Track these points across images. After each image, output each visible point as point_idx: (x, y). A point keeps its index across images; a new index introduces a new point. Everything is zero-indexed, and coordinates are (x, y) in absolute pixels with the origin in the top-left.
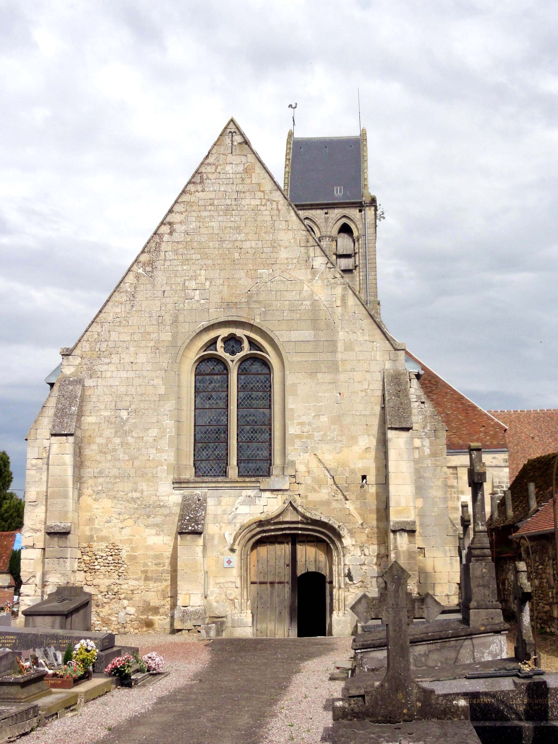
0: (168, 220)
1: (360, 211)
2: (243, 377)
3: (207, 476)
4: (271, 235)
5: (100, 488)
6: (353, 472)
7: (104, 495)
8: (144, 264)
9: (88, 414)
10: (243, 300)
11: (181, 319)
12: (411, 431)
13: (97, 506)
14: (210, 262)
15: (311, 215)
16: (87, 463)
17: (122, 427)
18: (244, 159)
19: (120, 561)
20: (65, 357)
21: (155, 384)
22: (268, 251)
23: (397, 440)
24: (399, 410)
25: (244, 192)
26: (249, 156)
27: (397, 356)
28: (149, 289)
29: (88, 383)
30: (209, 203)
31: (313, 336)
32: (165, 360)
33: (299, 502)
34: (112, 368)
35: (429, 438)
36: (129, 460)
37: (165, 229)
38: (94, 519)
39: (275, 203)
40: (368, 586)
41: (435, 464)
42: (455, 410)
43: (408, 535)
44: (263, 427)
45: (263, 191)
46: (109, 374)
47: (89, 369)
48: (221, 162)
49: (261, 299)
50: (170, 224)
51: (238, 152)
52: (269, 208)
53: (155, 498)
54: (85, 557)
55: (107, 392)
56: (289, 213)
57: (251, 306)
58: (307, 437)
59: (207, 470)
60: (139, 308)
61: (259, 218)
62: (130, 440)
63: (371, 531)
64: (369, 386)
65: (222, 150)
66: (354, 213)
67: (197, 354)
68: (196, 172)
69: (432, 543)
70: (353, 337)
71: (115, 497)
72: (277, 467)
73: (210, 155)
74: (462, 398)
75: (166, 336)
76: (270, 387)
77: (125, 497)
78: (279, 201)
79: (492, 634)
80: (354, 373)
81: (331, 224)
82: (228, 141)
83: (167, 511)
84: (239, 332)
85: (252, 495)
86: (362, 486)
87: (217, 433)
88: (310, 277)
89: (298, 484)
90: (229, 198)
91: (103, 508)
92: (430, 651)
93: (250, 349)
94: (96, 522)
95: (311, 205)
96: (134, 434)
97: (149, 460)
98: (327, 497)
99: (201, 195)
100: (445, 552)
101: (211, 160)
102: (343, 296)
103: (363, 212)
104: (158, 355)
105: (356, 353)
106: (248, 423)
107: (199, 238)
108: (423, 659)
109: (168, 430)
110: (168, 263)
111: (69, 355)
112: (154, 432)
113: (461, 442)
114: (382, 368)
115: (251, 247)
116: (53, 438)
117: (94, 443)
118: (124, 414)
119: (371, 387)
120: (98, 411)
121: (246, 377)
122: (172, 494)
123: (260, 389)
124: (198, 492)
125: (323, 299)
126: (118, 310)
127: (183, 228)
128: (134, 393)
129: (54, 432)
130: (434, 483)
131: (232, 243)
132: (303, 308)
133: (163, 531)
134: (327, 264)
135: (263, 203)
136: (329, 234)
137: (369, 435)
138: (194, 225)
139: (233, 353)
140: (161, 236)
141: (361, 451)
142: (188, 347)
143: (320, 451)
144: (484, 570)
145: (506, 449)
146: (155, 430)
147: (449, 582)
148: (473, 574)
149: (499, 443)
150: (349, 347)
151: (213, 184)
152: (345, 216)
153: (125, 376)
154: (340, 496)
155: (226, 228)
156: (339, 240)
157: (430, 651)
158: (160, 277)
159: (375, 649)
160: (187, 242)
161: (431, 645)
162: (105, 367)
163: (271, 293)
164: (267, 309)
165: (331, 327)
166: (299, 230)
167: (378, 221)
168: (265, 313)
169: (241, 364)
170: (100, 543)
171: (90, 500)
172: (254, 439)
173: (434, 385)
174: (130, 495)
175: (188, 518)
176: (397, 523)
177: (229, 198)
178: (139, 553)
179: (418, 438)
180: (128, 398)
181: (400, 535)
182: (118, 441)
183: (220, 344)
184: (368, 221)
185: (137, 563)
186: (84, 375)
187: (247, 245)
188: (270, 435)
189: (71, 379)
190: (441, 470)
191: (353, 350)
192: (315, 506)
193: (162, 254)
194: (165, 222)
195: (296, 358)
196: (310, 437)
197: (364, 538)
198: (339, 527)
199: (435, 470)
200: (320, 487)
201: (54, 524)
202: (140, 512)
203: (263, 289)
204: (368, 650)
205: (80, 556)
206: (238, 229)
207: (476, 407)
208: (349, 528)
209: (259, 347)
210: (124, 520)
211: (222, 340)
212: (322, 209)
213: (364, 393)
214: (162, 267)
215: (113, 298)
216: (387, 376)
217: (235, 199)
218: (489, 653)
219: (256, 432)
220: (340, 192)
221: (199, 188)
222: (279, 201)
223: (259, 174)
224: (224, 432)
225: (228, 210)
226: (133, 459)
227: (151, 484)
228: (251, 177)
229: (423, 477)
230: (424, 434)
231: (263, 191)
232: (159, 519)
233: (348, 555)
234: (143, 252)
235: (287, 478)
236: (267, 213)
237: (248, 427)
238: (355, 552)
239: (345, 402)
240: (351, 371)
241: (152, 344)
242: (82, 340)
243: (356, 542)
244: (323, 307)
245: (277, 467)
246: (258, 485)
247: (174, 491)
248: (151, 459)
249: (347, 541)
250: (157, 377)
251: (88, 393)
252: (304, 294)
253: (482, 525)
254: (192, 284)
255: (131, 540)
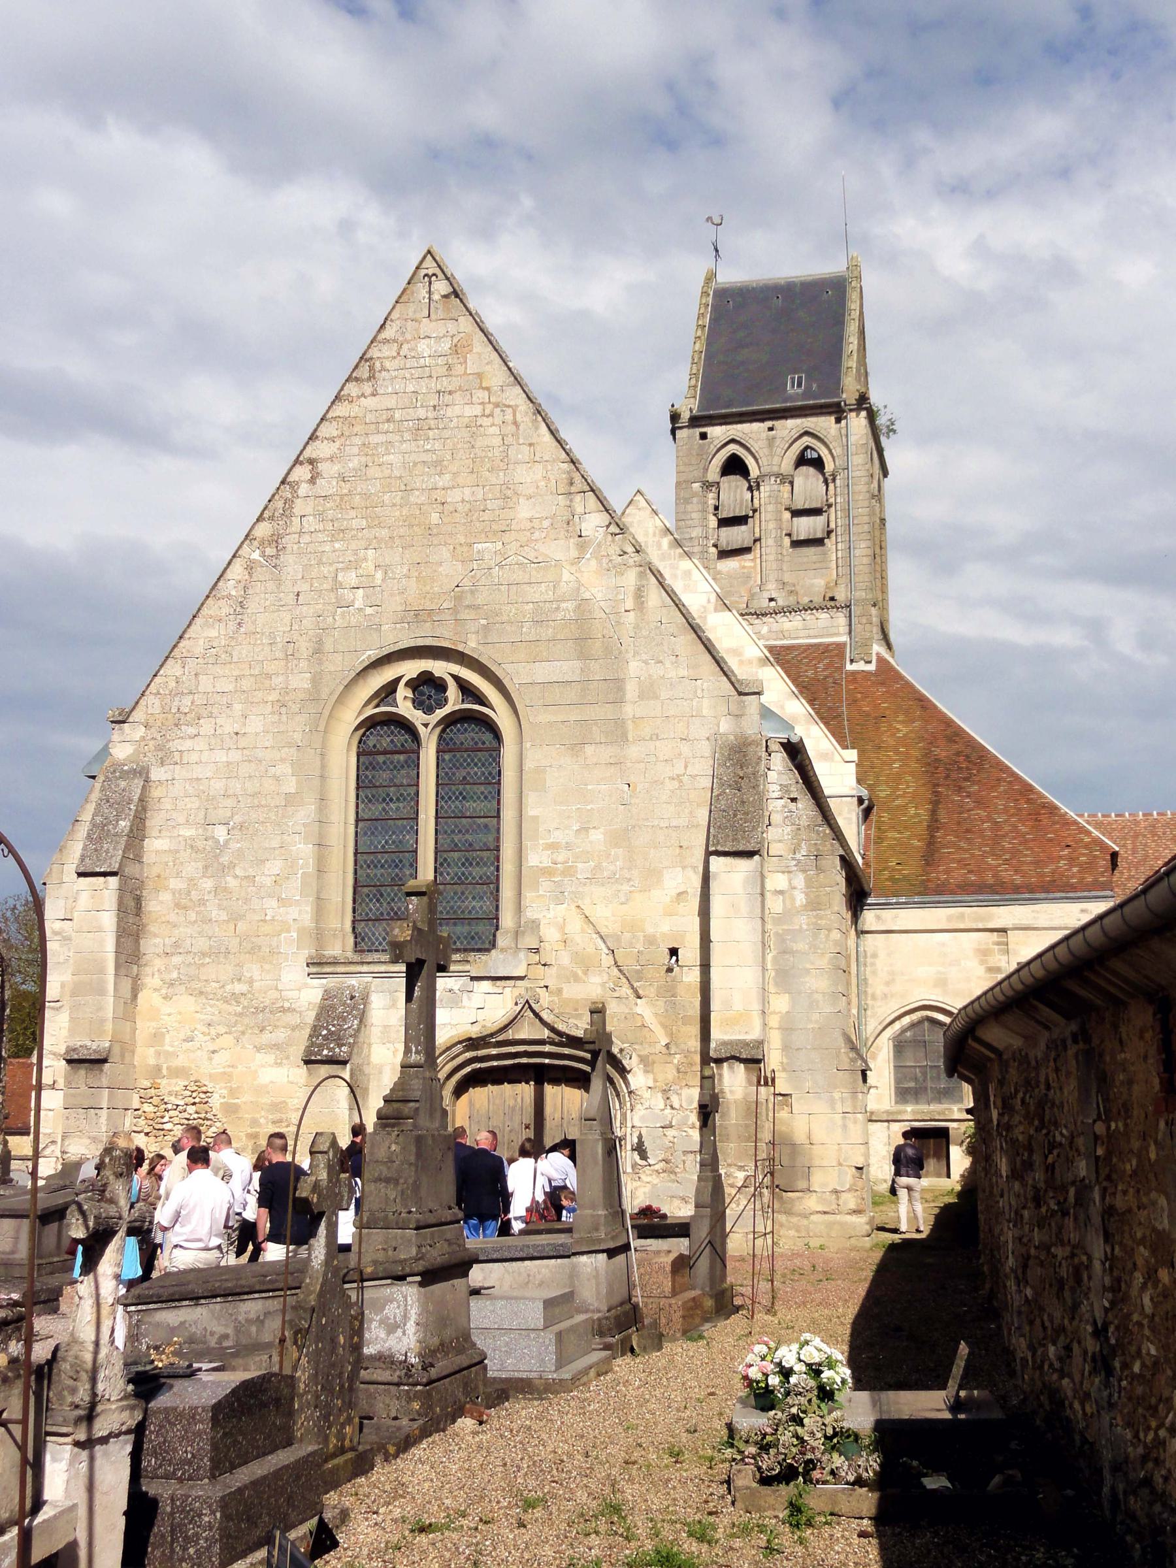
0: (307, 453)
1: (838, 421)
2: (447, 757)
3: (377, 951)
4: (501, 474)
5: (175, 975)
6: (651, 941)
7: (183, 988)
8: (262, 543)
9: (155, 833)
10: (445, 605)
11: (328, 646)
12: (757, 857)
13: (169, 1010)
14: (384, 533)
15: (740, 435)
16: (152, 928)
17: (216, 857)
18: (451, 327)
19: (209, 1116)
20: (117, 726)
21: (278, 774)
22: (495, 507)
23: (731, 875)
24: (735, 815)
25: (450, 393)
26: (461, 319)
27: (744, 707)
28: (269, 590)
29: (156, 774)
30: (384, 417)
31: (578, 672)
32: (297, 729)
33: (545, 1001)
34: (200, 744)
35: (804, 871)
36: (228, 921)
37: (302, 473)
38: (163, 1035)
39: (510, 411)
40: (677, 1170)
41: (816, 924)
42: (1012, 815)
43: (746, 1068)
44: (486, 854)
45: (488, 389)
46: (194, 757)
47: (159, 748)
48: (408, 336)
49: (479, 601)
50: (311, 462)
51: (441, 314)
52: (498, 421)
53: (276, 994)
54: (147, 1108)
55: (191, 791)
56: (537, 428)
57: (461, 616)
58: (564, 873)
59: (377, 939)
60: (252, 629)
61: (479, 443)
62: (231, 882)
63: (684, 1060)
64: (686, 767)
65: (410, 310)
66: (825, 424)
67: (360, 713)
68: (361, 358)
69: (808, 1085)
70: (656, 671)
71: (201, 993)
72: (507, 932)
73: (388, 322)
74: (1029, 789)
75: (301, 681)
76: (500, 775)
77: (220, 992)
78: (517, 406)
79: (389, 1281)
80: (658, 743)
81: (779, 450)
82: (424, 293)
83: (294, 1019)
84: (440, 668)
85: (456, 988)
86: (670, 970)
87: (397, 866)
88: (574, 553)
89: (544, 965)
90: (422, 406)
91: (180, 1013)
92: (269, 1313)
93: (463, 701)
94: (168, 1039)
95: (741, 414)
96: (239, 871)
97: (264, 921)
98: (599, 991)
99: (370, 402)
100: (832, 1103)
101: (388, 333)
102: (639, 589)
103: (844, 422)
104: (284, 718)
105: (663, 704)
106: (455, 848)
107: (364, 487)
108: (254, 1329)
109: (301, 862)
110: (306, 538)
111: (124, 722)
112: (275, 867)
113: (1018, 879)
114: (712, 731)
115: (463, 501)
116: (82, 879)
117: (166, 888)
118: (221, 833)
119: (690, 771)
120: (174, 827)
121: (454, 756)
122: (306, 986)
123: (479, 778)
124: (353, 981)
125: (599, 596)
126: (213, 633)
127: (336, 468)
128: (239, 791)
129: (82, 869)
130: (813, 964)
131: (426, 493)
132: (560, 616)
133: (288, 1058)
134: (608, 527)
135: (487, 412)
136: (775, 469)
137: (684, 868)
138: (356, 462)
139: (429, 710)
140: (294, 486)
141: (668, 899)
142: (341, 699)
143: (587, 901)
144: (394, 1147)
145: (1109, 893)
146: (277, 862)
147: (840, 1164)
148: (372, 1154)
149: (1096, 881)
150: (648, 692)
151: (393, 378)
152: (807, 433)
153: (224, 759)
154: (626, 991)
155: (415, 464)
156: (798, 482)
157: (267, 1314)
158: (291, 564)
159: (164, 1305)
160: (342, 496)
161: (270, 1301)
162: (188, 744)
163: (499, 590)
164: (491, 621)
165: (613, 653)
166: (554, 461)
167: (883, 439)
168: (486, 628)
169: (443, 731)
170: (174, 1081)
171: (156, 999)
172: (467, 878)
173: (975, 764)
174: (228, 987)
175: (325, 1032)
176: (724, 1043)
177: (422, 406)
178: (244, 1100)
179: (783, 872)
180: (230, 802)
181: (731, 1068)
182: (208, 884)
183: (402, 692)
184: (852, 439)
185: (239, 1118)
186: (150, 759)
187: (454, 496)
188: (498, 869)
189: (126, 768)
190: (827, 936)
191: (656, 697)
192: (576, 1010)
193: (296, 521)
194: (301, 458)
195: (544, 717)
196: (569, 872)
197: (670, 1073)
198: (621, 1050)
199: (815, 936)
200: (586, 973)
201: (79, 1043)
202: (246, 1021)
203: (483, 581)
204: (151, 1306)
205: (136, 1105)
206: (438, 465)
207: (1056, 808)
208: (642, 1053)
209: (478, 697)
210: (218, 1035)
211: (407, 684)
212: (762, 421)
213: (676, 784)
214: (295, 547)
215: (205, 611)
216: (721, 748)
217: (435, 407)
218: (381, 1322)
219: (471, 864)
220: (799, 385)
221: (367, 388)
222: (517, 406)
223: (479, 354)
224: (411, 865)
225: (419, 429)
226: (235, 918)
227: (267, 967)
228: (465, 362)
229: (792, 953)
230: (794, 863)
231: (488, 389)
232: (281, 1035)
233: (639, 1106)
234: (260, 519)
235: (522, 955)
236: (494, 430)
237: (456, 855)
238: (653, 1102)
239: (637, 801)
240: (651, 739)
241: (273, 696)
242: (147, 693)
243: (655, 1081)
244: (599, 614)
245: (507, 932)
246: (467, 967)
247: (309, 980)
248: (268, 918)
249: (638, 1079)
250: (283, 760)
251: (156, 793)
252: (564, 588)
253: (417, 1052)
254: (351, 578)
255: (230, 1075)
